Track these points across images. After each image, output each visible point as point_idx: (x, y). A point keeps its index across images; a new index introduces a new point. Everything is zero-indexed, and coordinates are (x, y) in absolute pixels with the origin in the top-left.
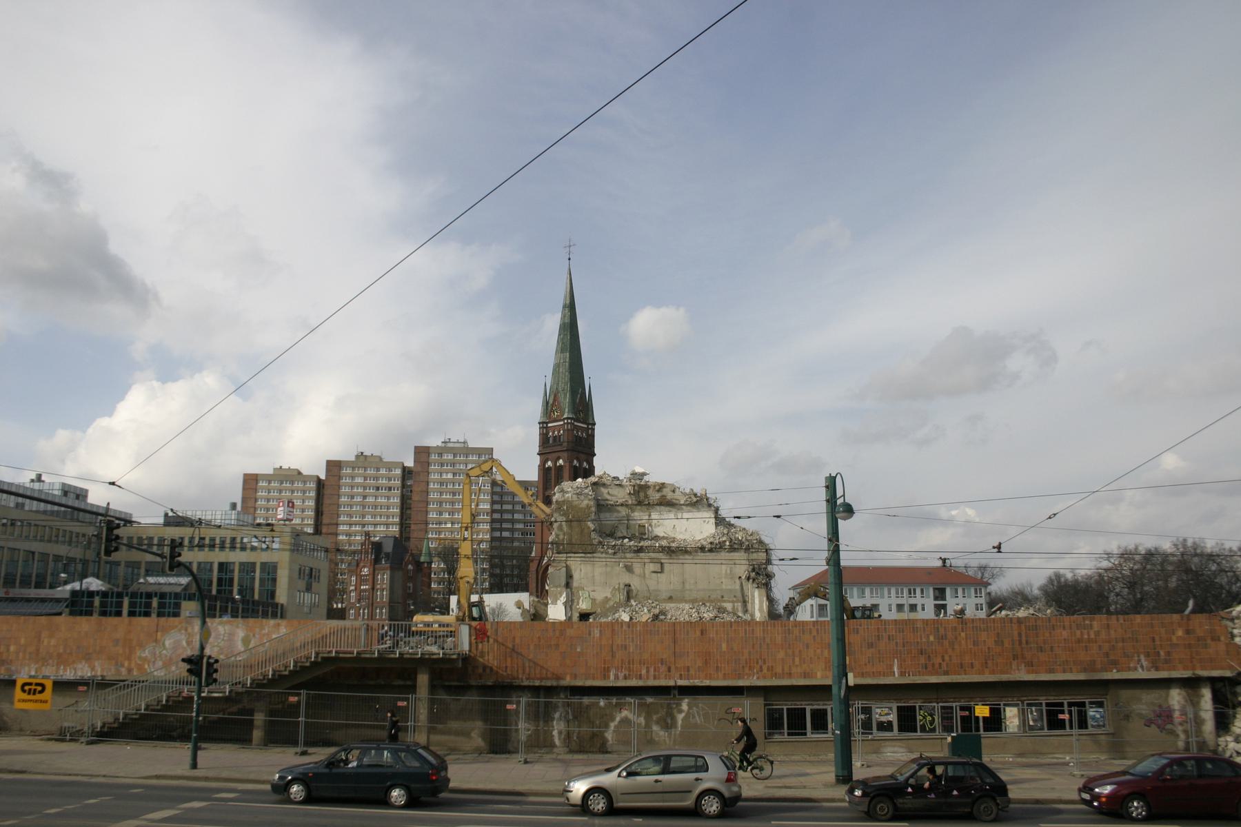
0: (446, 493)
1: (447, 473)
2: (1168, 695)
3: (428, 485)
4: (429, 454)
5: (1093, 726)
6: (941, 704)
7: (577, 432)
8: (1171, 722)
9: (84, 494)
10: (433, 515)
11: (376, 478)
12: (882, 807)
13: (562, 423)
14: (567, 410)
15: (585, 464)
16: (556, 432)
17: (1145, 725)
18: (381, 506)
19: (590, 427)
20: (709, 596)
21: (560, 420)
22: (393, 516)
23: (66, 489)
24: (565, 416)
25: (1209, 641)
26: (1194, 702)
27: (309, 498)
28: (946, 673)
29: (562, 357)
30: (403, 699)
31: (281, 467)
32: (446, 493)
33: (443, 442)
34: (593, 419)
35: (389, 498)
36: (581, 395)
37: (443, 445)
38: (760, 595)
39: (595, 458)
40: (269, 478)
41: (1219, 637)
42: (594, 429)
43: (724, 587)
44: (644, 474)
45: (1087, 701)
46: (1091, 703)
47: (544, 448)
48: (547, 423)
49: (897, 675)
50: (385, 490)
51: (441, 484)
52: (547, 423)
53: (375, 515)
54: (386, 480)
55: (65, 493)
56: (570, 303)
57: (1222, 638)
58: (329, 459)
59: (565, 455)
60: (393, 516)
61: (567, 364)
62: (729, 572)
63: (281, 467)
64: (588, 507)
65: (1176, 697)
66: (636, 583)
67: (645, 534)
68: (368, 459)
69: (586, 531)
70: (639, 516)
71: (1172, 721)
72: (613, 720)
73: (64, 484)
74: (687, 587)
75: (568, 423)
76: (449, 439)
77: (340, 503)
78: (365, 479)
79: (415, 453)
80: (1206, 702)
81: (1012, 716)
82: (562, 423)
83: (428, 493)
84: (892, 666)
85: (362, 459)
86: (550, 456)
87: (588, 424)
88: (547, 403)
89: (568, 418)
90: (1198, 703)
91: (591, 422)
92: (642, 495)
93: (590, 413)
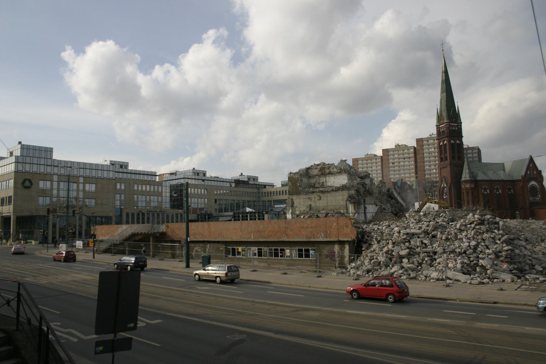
0: (432, 157)
1: (431, 148)
2: (334, 247)
3: (423, 155)
4: (423, 141)
5: (311, 257)
6: (269, 248)
7: (452, 128)
8: (334, 257)
9: (256, 178)
10: (427, 167)
11: (403, 154)
12: (390, 297)
13: (444, 125)
14: (445, 119)
15: (458, 142)
16: (443, 129)
17: (326, 257)
18: (407, 166)
19: (459, 124)
20: (336, 208)
21: (444, 124)
22: (412, 169)
23: (249, 177)
24: (445, 122)
25: (345, 227)
26: (342, 249)
27: (379, 165)
28: (265, 238)
29: (443, 95)
30: (142, 244)
31: (368, 154)
32: (432, 157)
33: (429, 135)
34: (460, 120)
35: (409, 162)
36: (453, 111)
37: (430, 136)
38: (351, 207)
39: (463, 138)
40: (362, 159)
41: (348, 226)
42: (461, 125)
43: (341, 204)
44: (345, 161)
45: (310, 248)
46: (311, 249)
47: (439, 137)
48: (439, 126)
49: (252, 238)
50: (408, 159)
51: (429, 153)
52: (439, 126)
53: (435, 165)
54: (407, 155)
55: (249, 179)
56: (445, 70)
57: (349, 226)
58: (104, 269)
59: (446, 139)
60: (412, 169)
61: (445, 98)
62: (342, 198)
63: (368, 154)
64: (298, 178)
65: (336, 248)
66: (313, 204)
67: (324, 185)
68: (400, 146)
69: (297, 186)
70: (322, 179)
71: (335, 256)
72: (194, 250)
73: (248, 176)
74: (329, 205)
75: (446, 125)
76: (433, 133)
77: (425, 161)
78: (399, 155)
79: (417, 142)
80: (346, 250)
81: (288, 252)
82: (444, 125)
83: (424, 158)
84: (251, 235)
85: (398, 147)
86: (441, 140)
87: (458, 123)
88: (439, 116)
89: (446, 123)
90: (344, 250)
91: (459, 122)
92: (323, 171)
93: (459, 118)
